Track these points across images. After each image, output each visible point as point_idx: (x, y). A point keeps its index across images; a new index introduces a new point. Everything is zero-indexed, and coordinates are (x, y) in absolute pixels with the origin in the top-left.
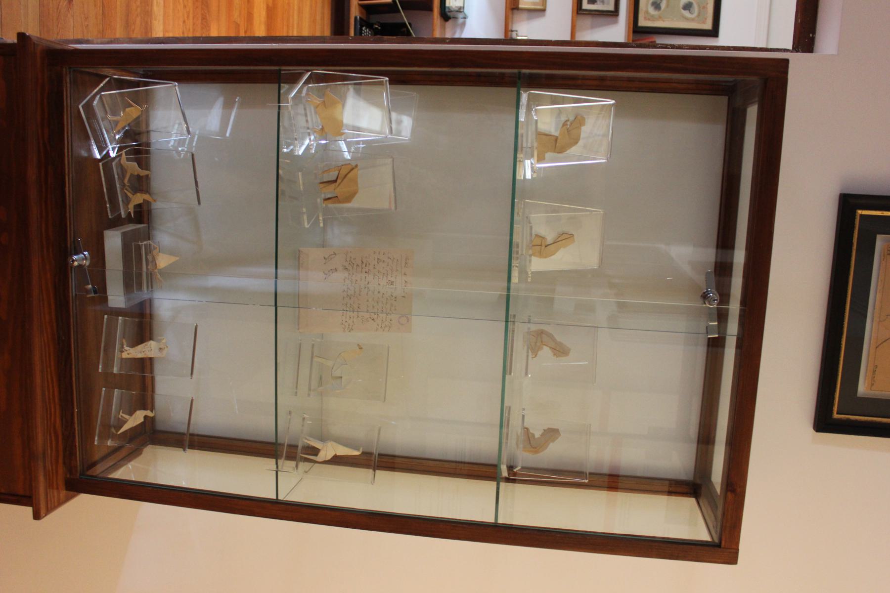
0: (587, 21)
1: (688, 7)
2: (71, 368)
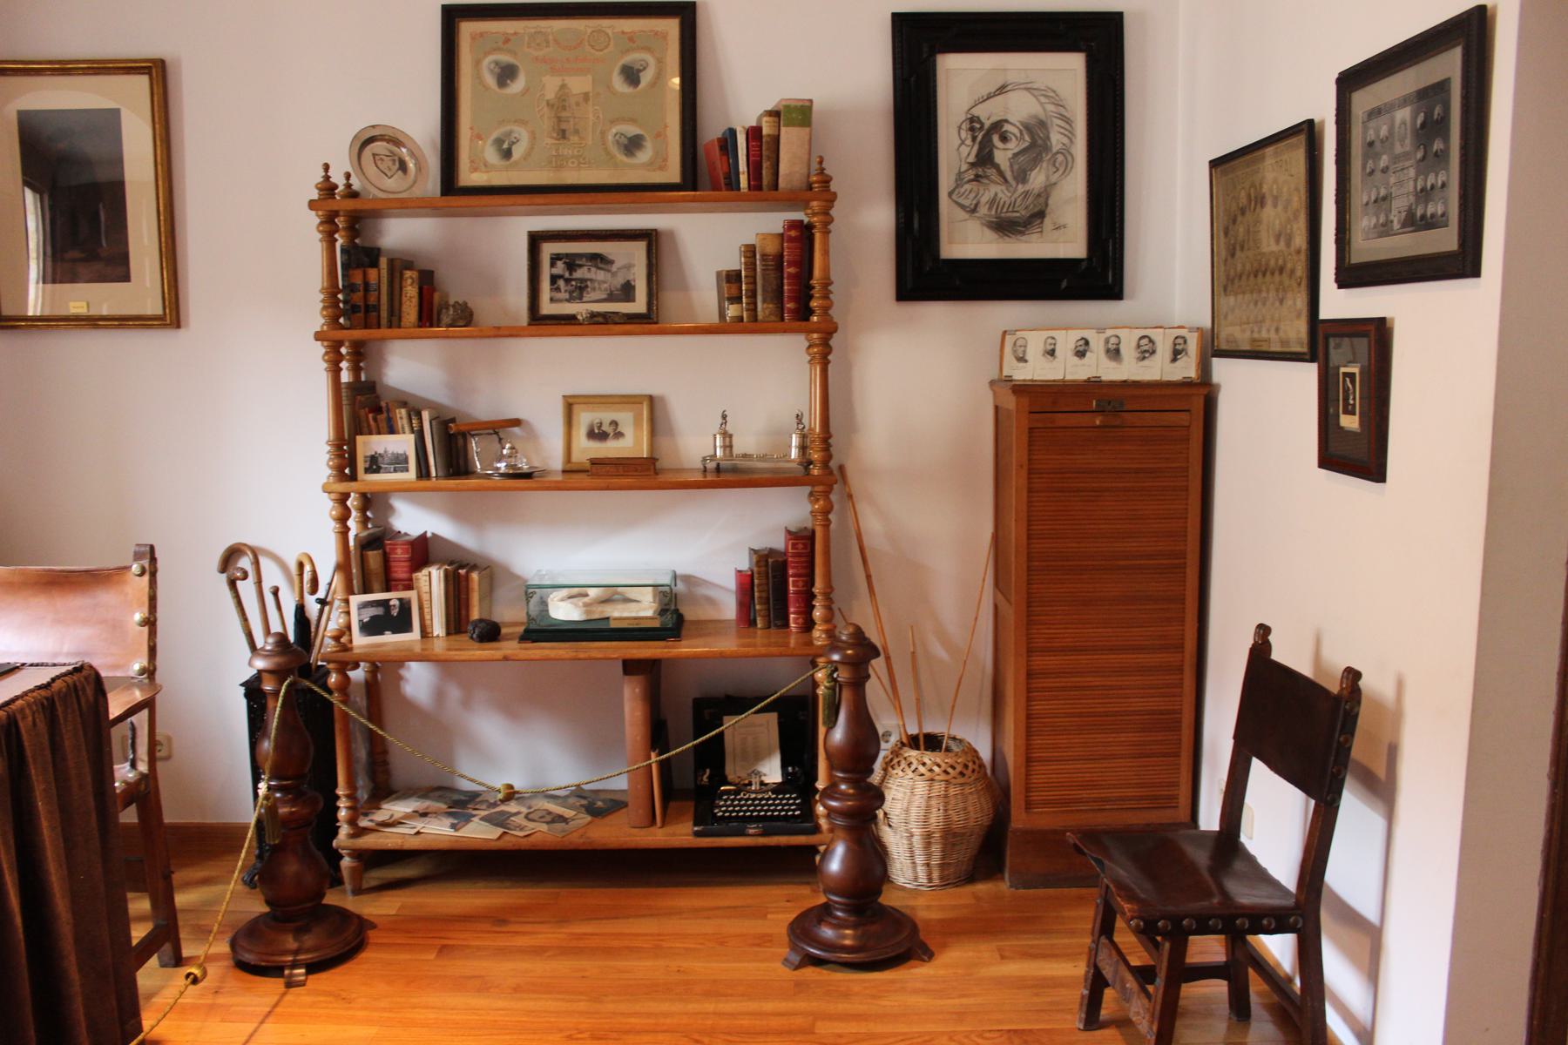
1: (631, 75)
2: (1032, 947)
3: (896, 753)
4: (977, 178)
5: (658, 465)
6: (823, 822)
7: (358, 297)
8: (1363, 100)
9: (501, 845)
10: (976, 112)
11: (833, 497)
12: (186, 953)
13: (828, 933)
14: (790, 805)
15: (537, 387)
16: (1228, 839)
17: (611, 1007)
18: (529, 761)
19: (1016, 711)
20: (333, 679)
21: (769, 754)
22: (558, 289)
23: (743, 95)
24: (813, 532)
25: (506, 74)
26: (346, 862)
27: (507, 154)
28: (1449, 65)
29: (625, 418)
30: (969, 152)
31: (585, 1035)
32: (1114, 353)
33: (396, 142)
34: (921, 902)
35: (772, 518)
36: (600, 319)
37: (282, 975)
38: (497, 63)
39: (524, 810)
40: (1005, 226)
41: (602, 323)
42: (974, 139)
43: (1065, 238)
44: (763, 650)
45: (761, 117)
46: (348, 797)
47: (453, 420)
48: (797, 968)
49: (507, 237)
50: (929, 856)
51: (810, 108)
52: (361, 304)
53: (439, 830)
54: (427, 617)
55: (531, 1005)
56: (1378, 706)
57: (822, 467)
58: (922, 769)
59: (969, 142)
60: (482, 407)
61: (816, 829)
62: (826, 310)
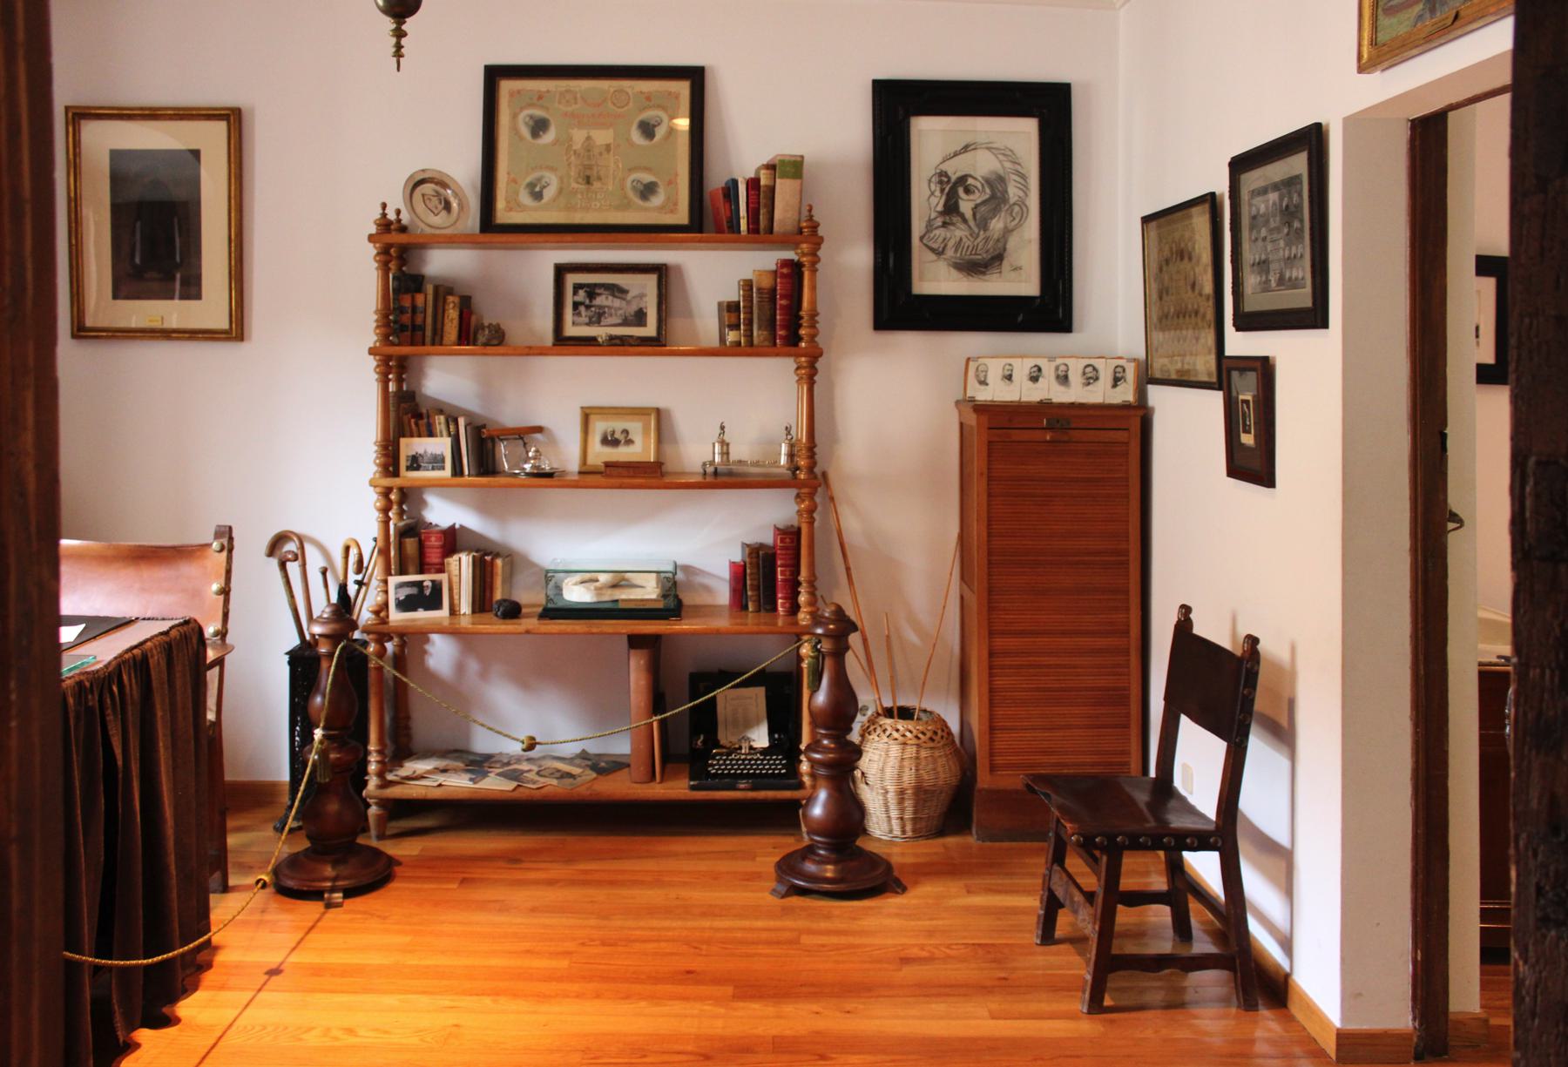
0: (677, 325)
1: (648, 130)
3: (872, 721)
4: (945, 225)
5: (664, 468)
6: (806, 779)
7: (406, 319)
8: (1253, 179)
9: (516, 795)
10: (944, 167)
11: (818, 499)
12: (232, 882)
13: (810, 867)
14: (778, 765)
15: (558, 399)
16: (1164, 787)
18: (535, 727)
19: (980, 686)
21: (758, 723)
22: (579, 314)
23: (743, 151)
24: (799, 529)
25: (539, 127)
26: (373, 810)
27: (538, 196)
28: (1298, 164)
29: (635, 427)
30: (938, 202)
32: (1064, 379)
33: (444, 185)
34: (896, 850)
35: (761, 517)
39: (536, 769)
40: (973, 267)
41: (619, 345)
42: (942, 191)
43: (1021, 278)
44: (755, 628)
45: (758, 171)
46: (380, 752)
47: (484, 426)
49: (536, 268)
50: (902, 810)
53: (459, 783)
55: (547, 921)
56: (1277, 667)
57: (807, 473)
58: (895, 735)
59: (938, 193)
60: (509, 415)
61: (801, 785)
62: (813, 337)
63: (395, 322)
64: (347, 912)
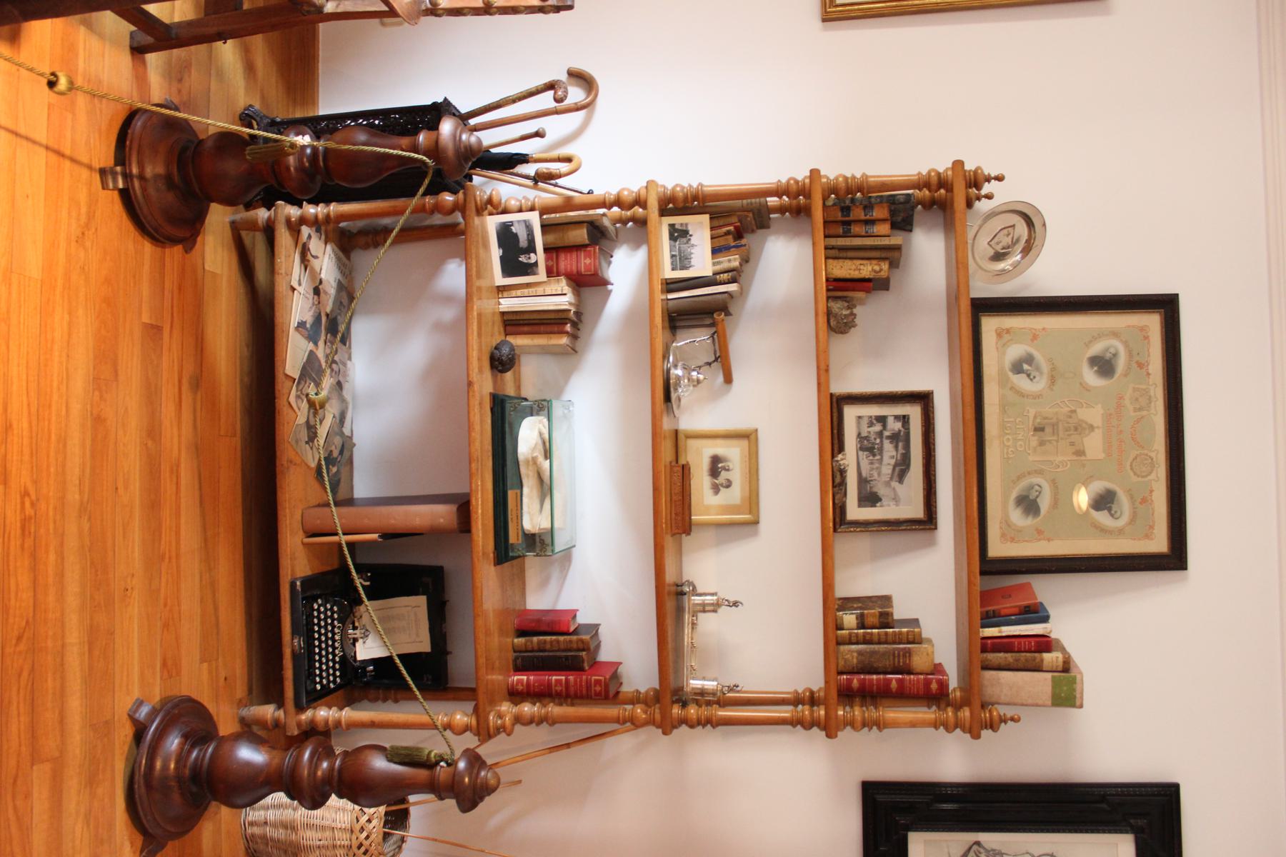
7: (858, 213)
9: (280, 377)
12: (151, 58)
13: (173, 743)
15: (762, 400)
17: (72, 529)
18: (382, 388)
20: (448, 198)
22: (871, 424)
23: (1081, 620)
25: (1104, 366)
26: (262, 214)
27: (1017, 368)
29: (734, 495)
31: (29, 510)
33: (1027, 250)
35: (628, 648)
36: (838, 480)
37: (116, 165)
38: (1115, 355)
41: (834, 481)
46: (328, 216)
47: (728, 314)
48: (132, 718)
49: (930, 371)
50: (274, 825)
51: (1073, 706)
52: (851, 218)
53: (297, 308)
54: (519, 293)
60: (745, 340)
62: (851, 723)
63: (853, 200)
64: (92, 202)
